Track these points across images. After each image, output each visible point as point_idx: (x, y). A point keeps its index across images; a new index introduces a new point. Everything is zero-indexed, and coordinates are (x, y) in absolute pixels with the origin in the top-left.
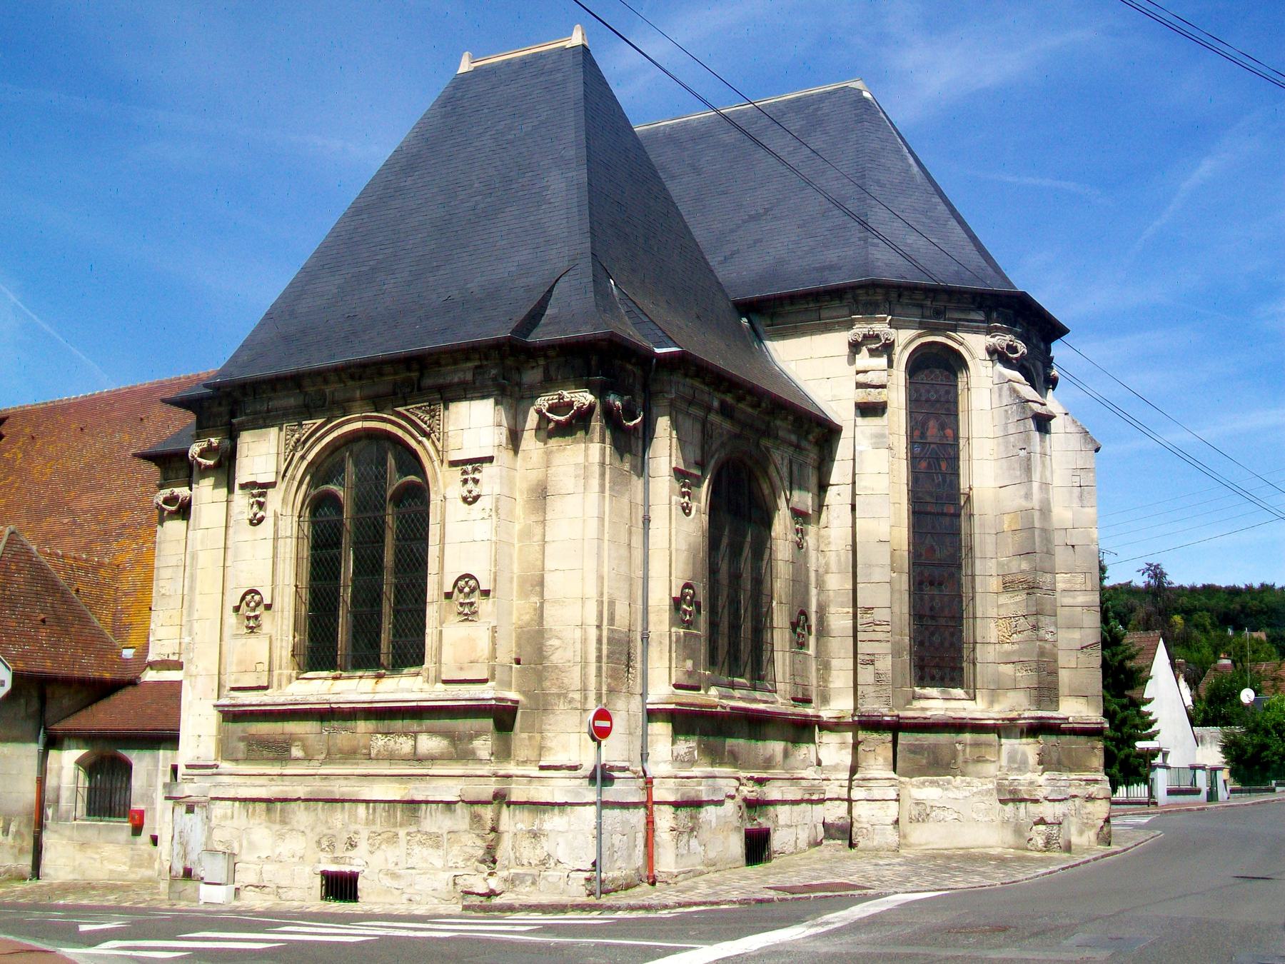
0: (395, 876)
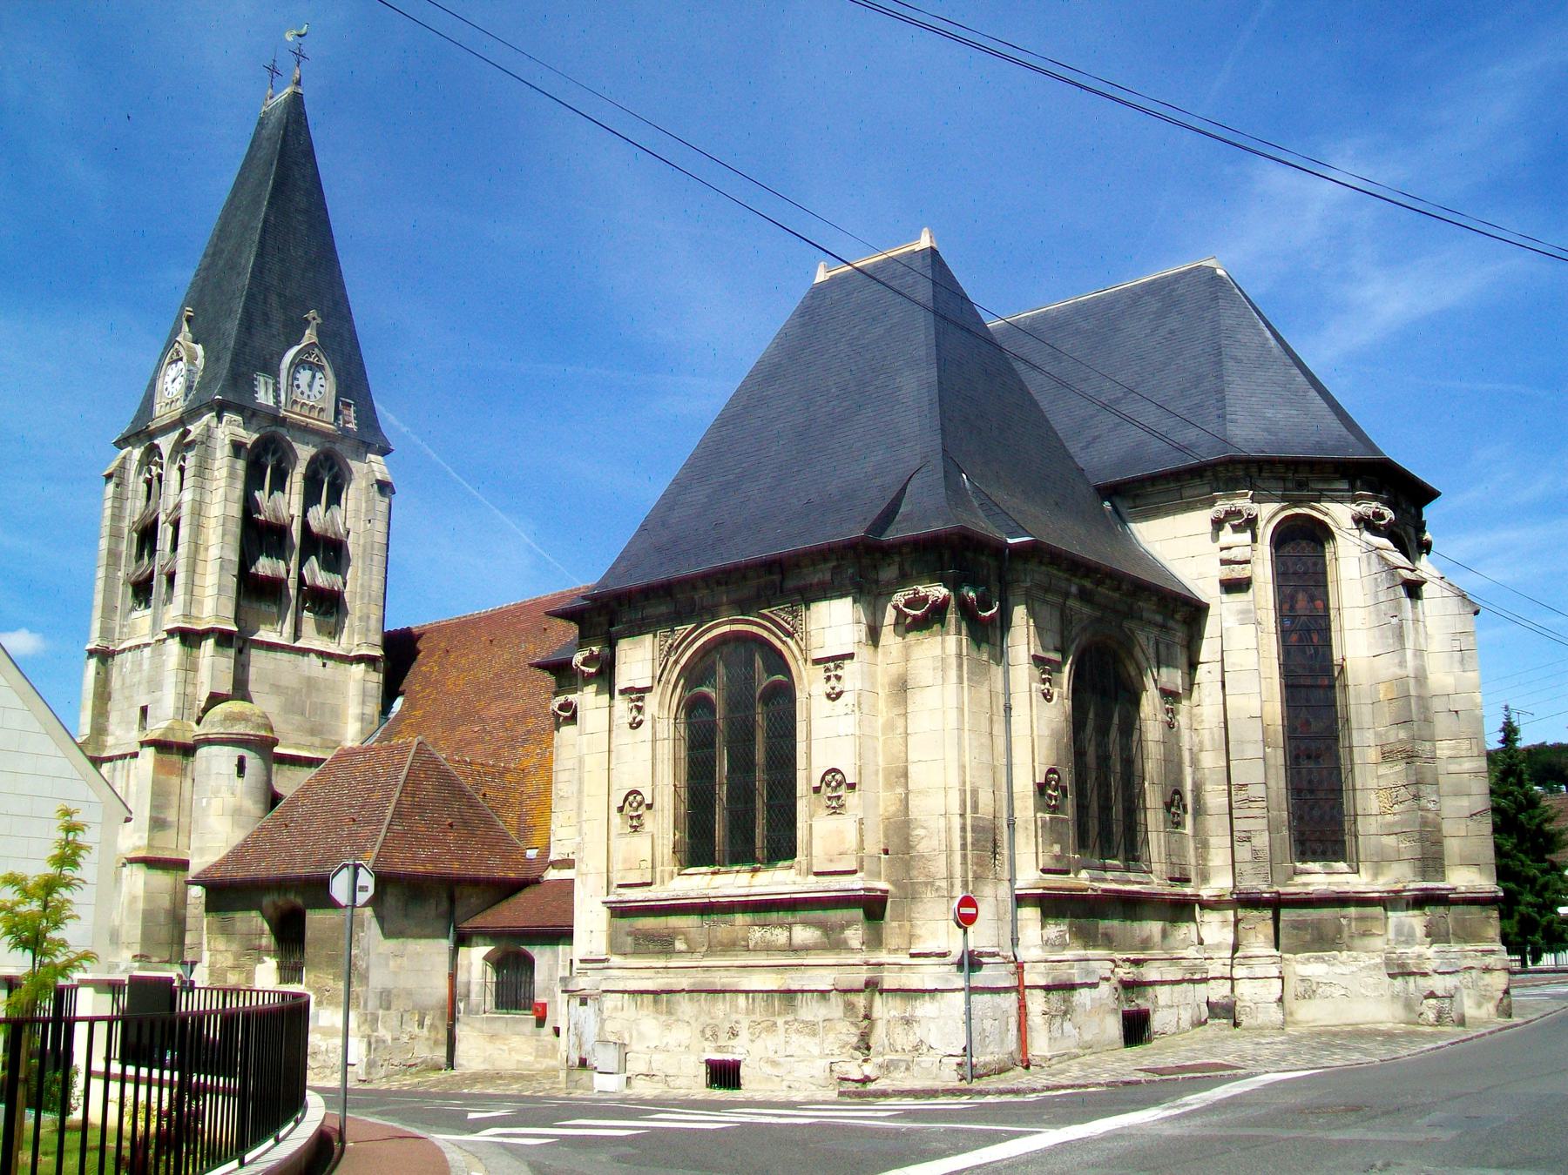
0: (774, 1063)
